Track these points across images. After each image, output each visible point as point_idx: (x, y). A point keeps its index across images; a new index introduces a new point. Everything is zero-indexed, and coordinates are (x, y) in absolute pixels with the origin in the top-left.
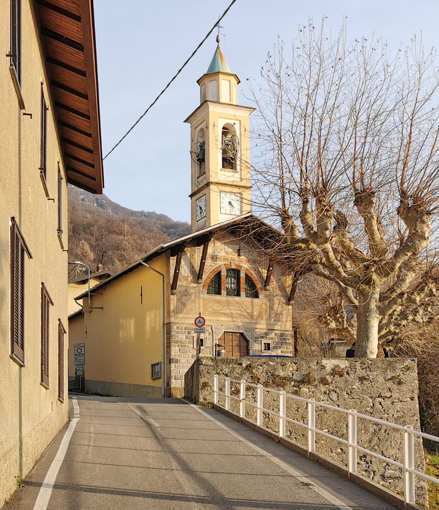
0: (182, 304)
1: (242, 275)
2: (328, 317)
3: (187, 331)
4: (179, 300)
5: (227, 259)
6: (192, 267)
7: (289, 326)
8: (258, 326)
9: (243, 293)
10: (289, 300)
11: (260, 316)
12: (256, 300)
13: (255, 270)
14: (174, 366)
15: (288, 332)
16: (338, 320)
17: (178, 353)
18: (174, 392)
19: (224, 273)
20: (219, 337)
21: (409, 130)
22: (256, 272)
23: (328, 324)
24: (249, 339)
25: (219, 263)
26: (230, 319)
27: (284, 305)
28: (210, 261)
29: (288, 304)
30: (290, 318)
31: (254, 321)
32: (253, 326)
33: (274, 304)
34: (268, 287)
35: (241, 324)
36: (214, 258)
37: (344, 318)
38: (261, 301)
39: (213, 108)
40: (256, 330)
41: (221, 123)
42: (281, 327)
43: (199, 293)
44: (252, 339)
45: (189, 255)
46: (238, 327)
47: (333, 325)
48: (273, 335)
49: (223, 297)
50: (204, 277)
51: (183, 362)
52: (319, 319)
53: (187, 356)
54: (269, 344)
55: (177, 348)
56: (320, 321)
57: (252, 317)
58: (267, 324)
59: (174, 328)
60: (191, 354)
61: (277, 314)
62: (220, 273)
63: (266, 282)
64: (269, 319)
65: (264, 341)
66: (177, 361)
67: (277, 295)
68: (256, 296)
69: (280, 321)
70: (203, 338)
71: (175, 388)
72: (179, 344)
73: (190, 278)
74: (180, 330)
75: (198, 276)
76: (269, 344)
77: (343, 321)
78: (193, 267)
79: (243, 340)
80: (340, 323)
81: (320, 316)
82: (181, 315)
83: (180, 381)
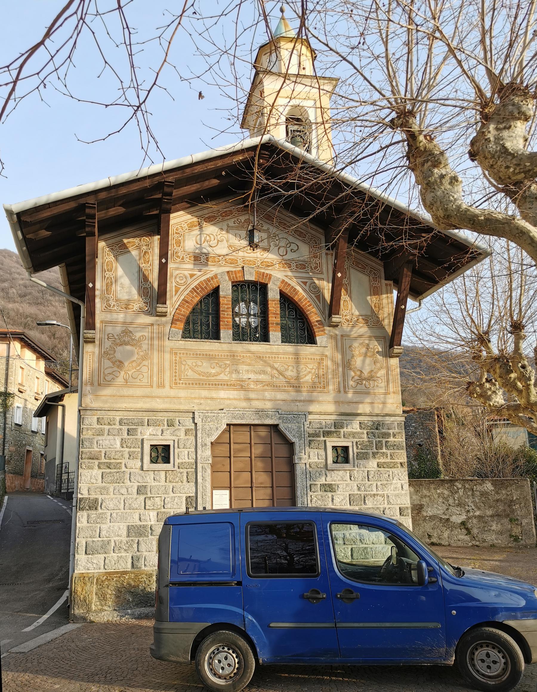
0: (114, 363)
1: (273, 295)
2: (488, 385)
3: (125, 428)
4: (104, 355)
5: (233, 262)
6: (143, 279)
7: (394, 404)
8: (313, 408)
9: (275, 334)
10: (391, 346)
12: (307, 350)
13: (305, 283)
14: (84, 520)
15: (392, 419)
16: (514, 386)
17: (100, 484)
18: (79, 589)
19: (226, 291)
20: (213, 438)
22: (307, 288)
23: (489, 398)
24: (293, 440)
25: (213, 270)
26: (242, 394)
27: (380, 358)
28: (191, 266)
29: (388, 353)
30: (395, 387)
31: (304, 395)
32: (301, 407)
33: (353, 356)
34: (335, 319)
35: (268, 405)
36: (200, 259)
37: (529, 379)
40: (310, 417)
42: (373, 408)
43: (160, 337)
44: (300, 437)
45: (134, 253)
46: (259, 412)
47: (499, 399)
48: (354, 426)
49: (225, 345)
51: (111, 506)
52: (467, 389)
53: (124, 491)
54: (346, 449)
55: (97, 472)
56: (471, 394)
58: (337, 402)
60: (136, 485)
61: (361, 380)
62: (216, 290)
63: (332, 308)
64: (343, 388)
65: (331, 442)
66: (94, 505)
67: (360, 336)
68: (311, 340)
69: (368, 393)
70: (171, 443)
71: (83, 577)
72: (103, 460)
73: (138, 303)
74: (107, 427)
75: (155, 296)
76: (346, 449)
77: (527, 387)
78: (145, 279)
79: (279, 441)
80: (520, 392)
81: (470, 384)
82: (107, 391)
83: (102, 556)
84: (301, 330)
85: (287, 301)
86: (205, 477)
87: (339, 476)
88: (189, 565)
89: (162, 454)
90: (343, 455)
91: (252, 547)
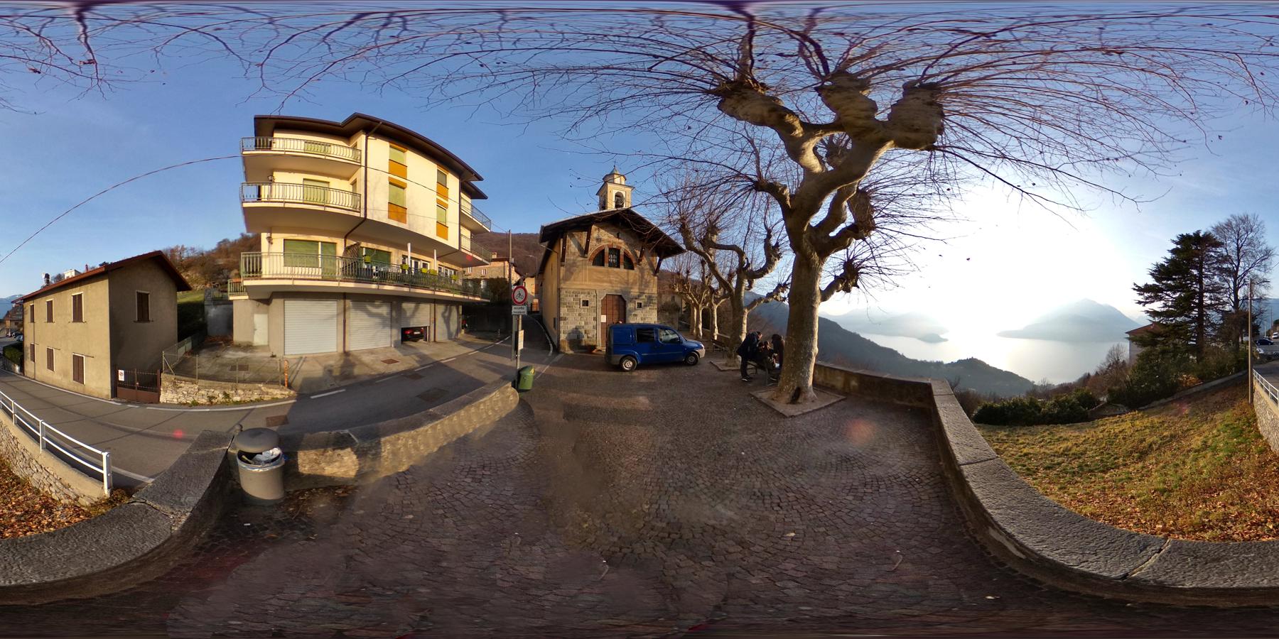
1: (622, 253)
6: (579, 246)
7: (655, 290)
11: (634, 283)
19: (607, 250)
21: (1086, 59)
36: (599, 240)
38: (635, 273)
39: (609, 185)
41: (614, 192)
50: (590, 253)
57: (627, 283)
59: (563, 292)
63: (640, 260)
75: (584, 252)
84: (630, 266)
85: (626, 256)
86: (599, 311)
87: (639, 312)
88: (50, 304)
89: (586, 303)
90: (640, 306)
91: (820, 380)
